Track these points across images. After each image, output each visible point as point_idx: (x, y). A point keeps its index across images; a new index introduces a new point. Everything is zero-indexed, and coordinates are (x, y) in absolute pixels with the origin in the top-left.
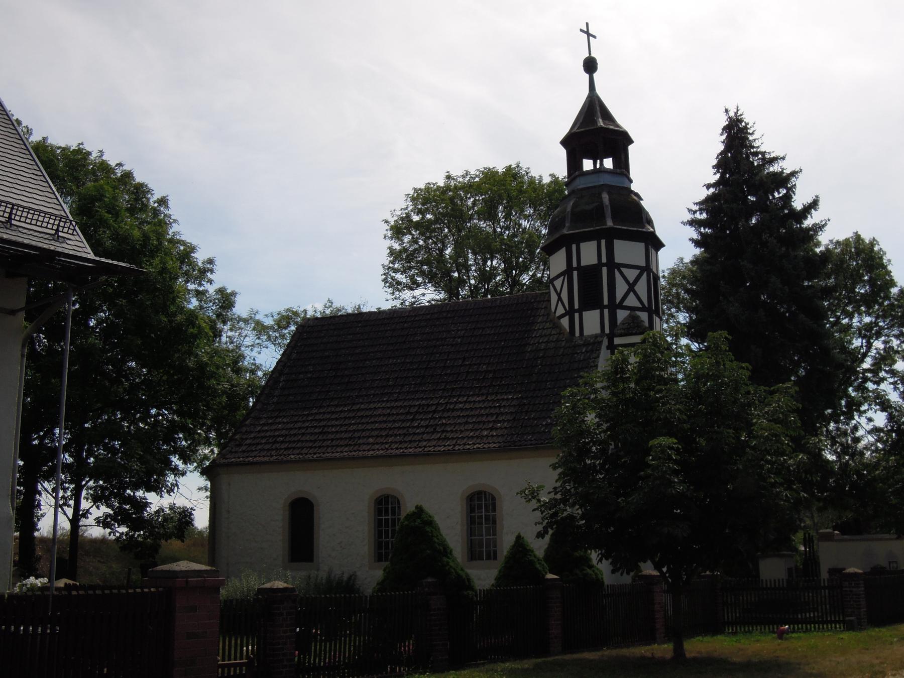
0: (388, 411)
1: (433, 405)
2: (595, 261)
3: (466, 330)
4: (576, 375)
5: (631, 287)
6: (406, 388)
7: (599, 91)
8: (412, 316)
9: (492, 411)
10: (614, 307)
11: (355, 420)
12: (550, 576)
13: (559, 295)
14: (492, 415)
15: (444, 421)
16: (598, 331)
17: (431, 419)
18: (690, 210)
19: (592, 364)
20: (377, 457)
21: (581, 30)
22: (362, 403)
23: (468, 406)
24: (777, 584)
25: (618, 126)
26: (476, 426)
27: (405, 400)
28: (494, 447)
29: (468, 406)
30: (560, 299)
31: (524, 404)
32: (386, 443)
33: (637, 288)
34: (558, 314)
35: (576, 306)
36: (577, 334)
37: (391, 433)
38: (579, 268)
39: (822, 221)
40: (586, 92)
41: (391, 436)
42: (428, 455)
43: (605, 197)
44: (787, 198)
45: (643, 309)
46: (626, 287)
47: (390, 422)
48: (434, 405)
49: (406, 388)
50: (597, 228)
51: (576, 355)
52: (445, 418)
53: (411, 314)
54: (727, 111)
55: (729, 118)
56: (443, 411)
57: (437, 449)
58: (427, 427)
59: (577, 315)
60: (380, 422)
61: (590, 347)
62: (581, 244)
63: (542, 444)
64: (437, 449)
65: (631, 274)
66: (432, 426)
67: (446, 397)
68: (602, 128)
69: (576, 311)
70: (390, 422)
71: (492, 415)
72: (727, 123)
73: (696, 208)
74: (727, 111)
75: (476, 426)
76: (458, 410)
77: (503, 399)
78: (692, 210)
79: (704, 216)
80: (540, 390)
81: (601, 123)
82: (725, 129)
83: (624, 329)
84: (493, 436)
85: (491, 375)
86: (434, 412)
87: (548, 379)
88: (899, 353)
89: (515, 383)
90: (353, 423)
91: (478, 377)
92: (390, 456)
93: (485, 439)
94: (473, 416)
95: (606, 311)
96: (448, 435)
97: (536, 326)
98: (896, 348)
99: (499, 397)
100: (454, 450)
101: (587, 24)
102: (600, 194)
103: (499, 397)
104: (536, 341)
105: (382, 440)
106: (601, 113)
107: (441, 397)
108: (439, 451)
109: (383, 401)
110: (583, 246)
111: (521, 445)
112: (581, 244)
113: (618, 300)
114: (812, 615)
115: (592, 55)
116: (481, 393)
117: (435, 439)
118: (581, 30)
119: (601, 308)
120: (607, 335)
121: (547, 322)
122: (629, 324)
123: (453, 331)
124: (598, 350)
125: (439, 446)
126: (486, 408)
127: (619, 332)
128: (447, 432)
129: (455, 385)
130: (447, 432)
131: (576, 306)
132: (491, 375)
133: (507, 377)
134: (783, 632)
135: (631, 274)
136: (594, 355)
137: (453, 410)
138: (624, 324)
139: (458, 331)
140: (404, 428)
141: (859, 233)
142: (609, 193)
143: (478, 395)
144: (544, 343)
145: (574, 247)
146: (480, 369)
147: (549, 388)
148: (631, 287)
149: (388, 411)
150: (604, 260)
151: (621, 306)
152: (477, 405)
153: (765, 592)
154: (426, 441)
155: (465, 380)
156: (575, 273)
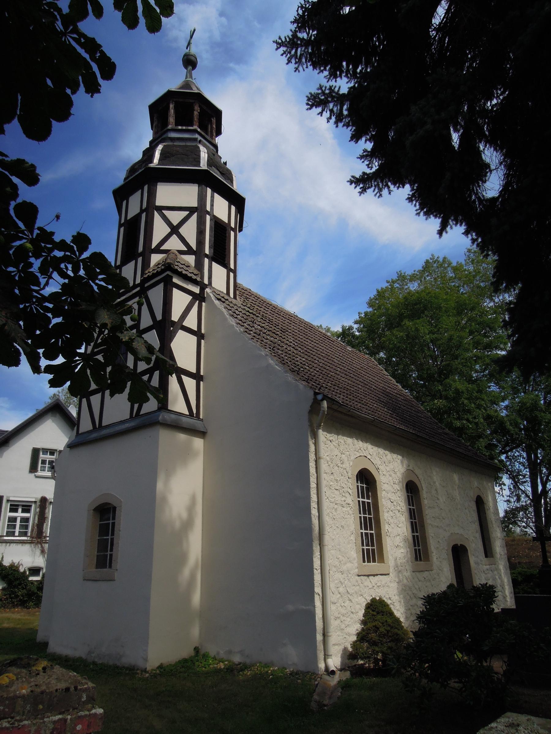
65: (175, 217)
148: (175, 230)
151: (158, 250)
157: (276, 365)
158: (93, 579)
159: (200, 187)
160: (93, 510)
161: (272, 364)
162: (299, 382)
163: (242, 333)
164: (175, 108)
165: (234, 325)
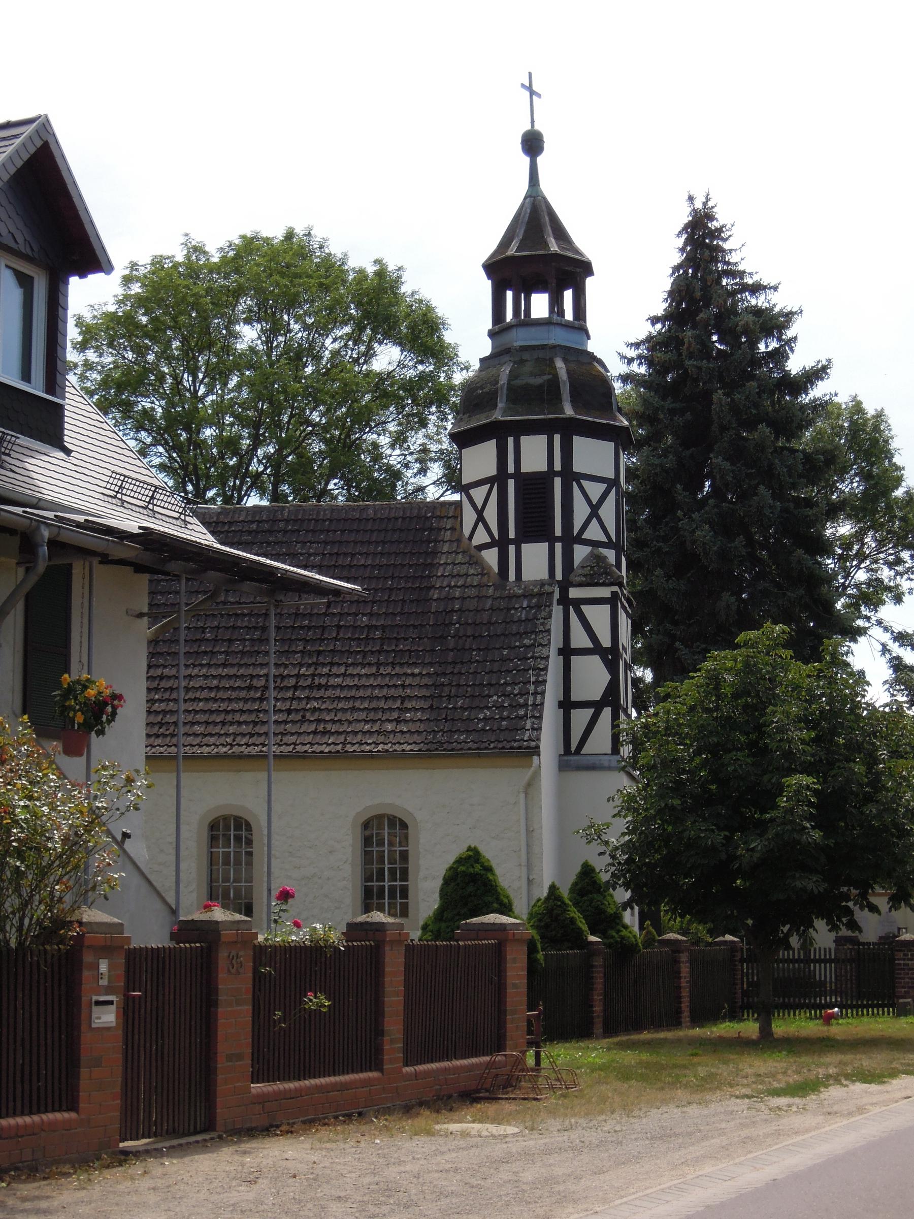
0: (215, 682)
1: (289, 676)
3: (324, 555)
4: (517, 644)
6: (237, 646)
7: (547, 188)
8: (224, 523)
9: (392, 692)
10: (570, 539)
11: (160, 694)
12: (593, 938)
13: (480, 513)
14: (394, 698)
15: (315, 704)
16: (545, 576)
17: (293, 699)
18: (623, 357)
19: (542, 628)
20: (218, 757)
22: (165, 667)
23: (349, 682)
25: (577, 251)
26: (372, 716)
27: (240, 666)
28: (412, 750)
29: (349, 682)
30: (481, 518)
31: (443, 685)
32: (227, 735)
33: (601, 512)
34: (476, 541)
35: (512, 535)
36: (512, 577)
37: (229, 718)
38: (518, 475)
39: (825, 395)
40: (522, 187)
41: (232, 723)
42: (304, 757)
43: (560, 364)
44: (779, 356)
45: (609, 545)
46: (588, 510)
47: (223, 700)
48: (292, 676)
49: (237, 646)
50: (550, 416)
51: (513, 612)
52: (315, 699)
53: (222, 518)
54: (691, 199)
55: (694, 210)
56: (310, 687)
57: (316, 748)
58: (289, 712)
59: (512, 549)
60: (207, 700)
61: (534, 601)
62: (522, 437)
63: (486, 748)
64: (316, 748)
65: (595, 490)
66: (297, 711)
67: (309, 666)
68: (556, 255)
70: (223, 700)
71: (394, 698)
72: (690, 218)
73: (632, 353)
74: (691, 199)
75: (372, 716)
76: (334, 687)
77: (406, 674)
78: (626, 357)
79: (643, 370)
80: (462, 663)
81: (554, 247)
82: (685, 228)
83: (585, 576)
84: (402, 732)
85: (378, 634)
86: (295, 687)
87: (474, 647)
88: (891, 591)
89: (420, 649)
90: (158, 700)
91: (357, 636)
92: (240, 757)
93: (392, 736)
94: (362, 698)
95: (558, 546)
96: (329, 727)
97: (440, 559)
98: (886, 581)
99: (398, 670)
100: (347, 752)
101: (530, 74)
102: (552, 361)
103: (398, 670)
104: (445, 584)
105: (217, 729)
106: (552, 227)
107: (301, 665)
108: (322, 752)
109: (202, 665)
110: (527, 442)
111: (453, 750)
112: (522, 437)
113: (576, 531)
114: (828, 998)
115: (537, 127)
116: (367, 661)
117: (309, 733)
119: (551, 539)
120: (558, 581)
121: (457, 553)
122: (592, 568)
123: (302, 554)
124: (549, 606)
125: (317, 743)
126: (381, 687)
127: (578, 579)
128: (326, 722)
129: (320, 645)
130: (326, 722)
131: (512, 535)
132: (378, 634)
133: (406, 639)
134: (832, 1016)
136: (544, 614)
137: (327, 687)
138: (583, 567)
139: (310, 555)
140: (250, 711)
141: (859, 398)
142: (565, 360)
143: (363, 666)
144: (458, 587)
145: (511, 440)
146: (359, 623)
147: (477, 661)
149: (215, 682)
150: (558, 467)
152: (364, 681)
153: (791, 966)
154: (292, 734)
155: (336, 639)
156: (511, 483)
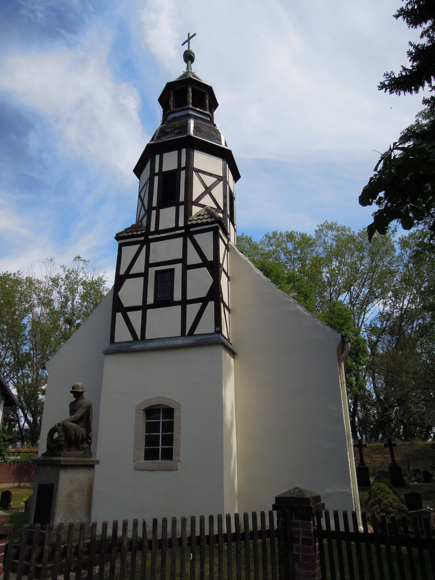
2: (175, 167)
5: (208, 190)
21: (189, 34)
24: (169, 529)
59: (154, 212)
65: (209, 181)
69: (154, 208)
101: (195, 35)
110: (166, 156)
118: (189, 34)
131: (155, 204)
135: (209, 181)
148: (208, 190)
151: (196, 203)
157: (304, 311)
158: (148, 469)
159: (223, 162)
160: (143, 410)
161: (301, 310)
162: (327, 327)
163: (269, 282)
164: (192, 92)
165: (261, 275)
